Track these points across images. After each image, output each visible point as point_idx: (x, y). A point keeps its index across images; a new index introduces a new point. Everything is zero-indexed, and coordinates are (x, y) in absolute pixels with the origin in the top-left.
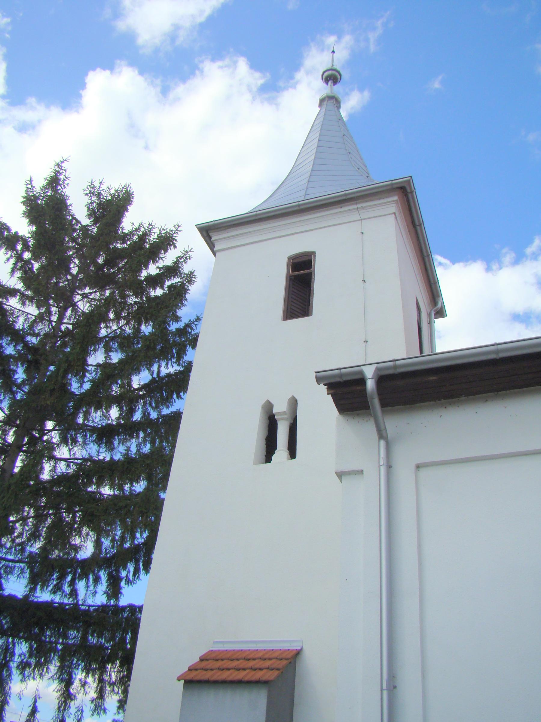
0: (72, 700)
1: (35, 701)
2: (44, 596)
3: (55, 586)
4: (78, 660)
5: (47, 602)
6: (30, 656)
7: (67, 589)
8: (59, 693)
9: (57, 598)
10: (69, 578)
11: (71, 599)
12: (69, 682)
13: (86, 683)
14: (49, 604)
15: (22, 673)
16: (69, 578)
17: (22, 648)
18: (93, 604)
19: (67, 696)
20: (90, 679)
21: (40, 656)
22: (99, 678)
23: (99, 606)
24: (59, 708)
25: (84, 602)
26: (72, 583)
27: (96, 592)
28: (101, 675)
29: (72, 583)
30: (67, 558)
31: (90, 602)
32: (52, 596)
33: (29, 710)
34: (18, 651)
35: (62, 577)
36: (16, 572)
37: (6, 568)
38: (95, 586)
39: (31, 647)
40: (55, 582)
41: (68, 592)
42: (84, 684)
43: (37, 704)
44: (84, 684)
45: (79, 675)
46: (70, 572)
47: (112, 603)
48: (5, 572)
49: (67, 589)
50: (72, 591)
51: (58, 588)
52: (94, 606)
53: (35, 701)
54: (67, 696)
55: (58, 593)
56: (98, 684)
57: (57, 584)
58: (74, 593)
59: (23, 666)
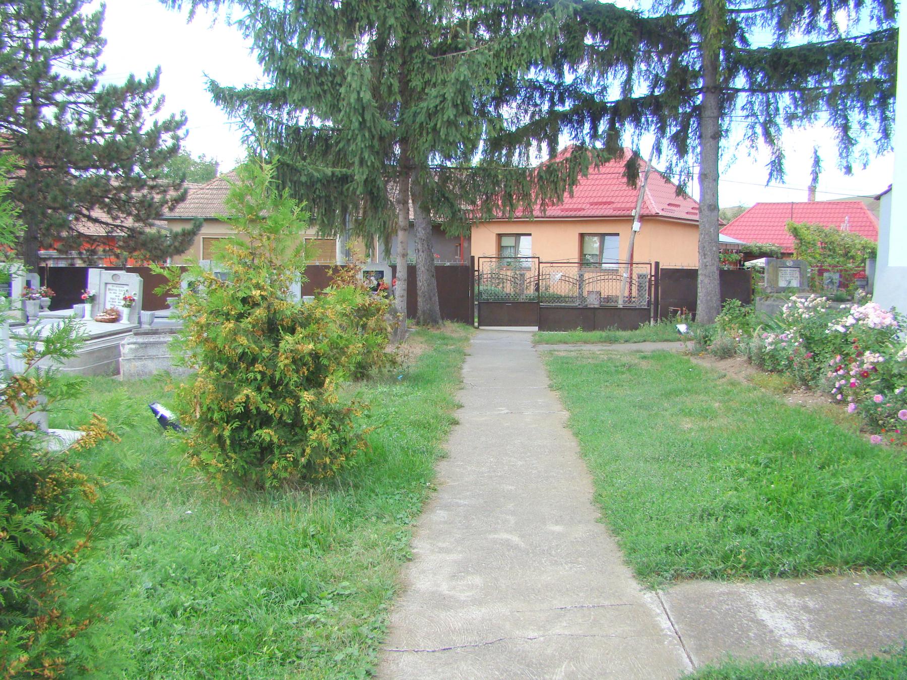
0: (853, 145)
1: (816, 152)
2: (796, 39)
3: (808, 25)
4: (853, 101)
5: (801, 48)
6: (796, 108)
7: (823, 24)
8: (838, 140)
9: (814, 38)
10: (824, 11)
11: (831, 36)
12: (845, 128)
13: (866, 124)
14: (810, 47)
15: (790, 125)
16: (824, 11)
17: (785, 100)
18: (859, 34)
19: (847, 141)
20: (345, 49)
21: (808, 103)
22: (881, 116)
23: (868, 35)
24: (841, 154)
25: (848, 34)
26: (829, 16)
27: (858, 20)
28: (883, 113)
29: (829, 16)
30: (13, 502)
31: (854, 33)
32: (806, 37)
33: (812, 161)
34: (781, 105)
35: (814, 13)
36: (759, 21)
37: (746, 20)
38: (857, 12)
39: (794, 99)
40: (807, 21)
41: (826, 28)
42: (864, 126)
43: (818, 154)
44: (864, 126)
45: (855, 116)
46: (824, 4)
47: (885, 28)
48: (747, 25)
49: (823, 24)
50: (830, 26)
51: (811, 27)
52: (861, 37)
53: (816, 152)
54: (847, 141)
55: (813, 33)
56: (881, 123)
57: (810, 22)
58: (833, 27)
59: (790, 118)
